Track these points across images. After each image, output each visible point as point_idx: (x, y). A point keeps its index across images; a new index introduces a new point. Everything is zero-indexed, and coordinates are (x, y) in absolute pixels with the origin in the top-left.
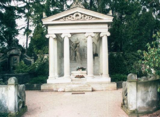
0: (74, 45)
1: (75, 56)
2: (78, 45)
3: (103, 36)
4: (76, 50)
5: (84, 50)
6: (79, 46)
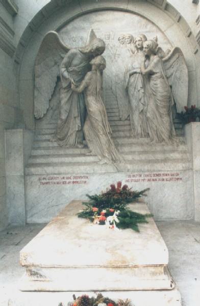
0: (75, 62)
1: (83, 121)
2: (96, 61)
3: (144, 203)
4: (86, 88)
5: (127, 90)
6: (101, 67)
